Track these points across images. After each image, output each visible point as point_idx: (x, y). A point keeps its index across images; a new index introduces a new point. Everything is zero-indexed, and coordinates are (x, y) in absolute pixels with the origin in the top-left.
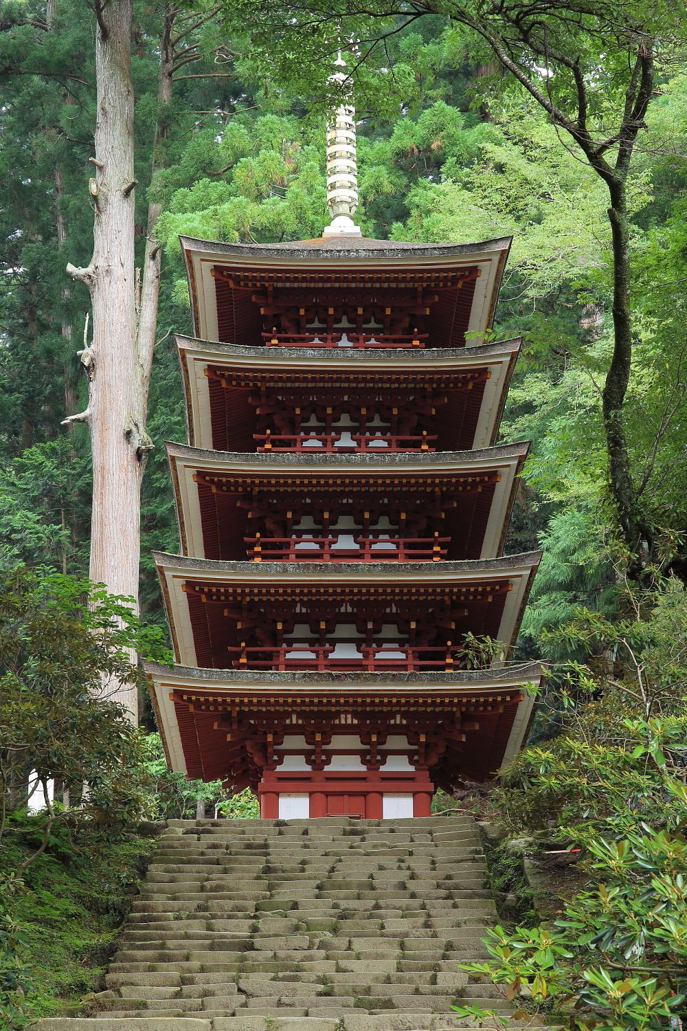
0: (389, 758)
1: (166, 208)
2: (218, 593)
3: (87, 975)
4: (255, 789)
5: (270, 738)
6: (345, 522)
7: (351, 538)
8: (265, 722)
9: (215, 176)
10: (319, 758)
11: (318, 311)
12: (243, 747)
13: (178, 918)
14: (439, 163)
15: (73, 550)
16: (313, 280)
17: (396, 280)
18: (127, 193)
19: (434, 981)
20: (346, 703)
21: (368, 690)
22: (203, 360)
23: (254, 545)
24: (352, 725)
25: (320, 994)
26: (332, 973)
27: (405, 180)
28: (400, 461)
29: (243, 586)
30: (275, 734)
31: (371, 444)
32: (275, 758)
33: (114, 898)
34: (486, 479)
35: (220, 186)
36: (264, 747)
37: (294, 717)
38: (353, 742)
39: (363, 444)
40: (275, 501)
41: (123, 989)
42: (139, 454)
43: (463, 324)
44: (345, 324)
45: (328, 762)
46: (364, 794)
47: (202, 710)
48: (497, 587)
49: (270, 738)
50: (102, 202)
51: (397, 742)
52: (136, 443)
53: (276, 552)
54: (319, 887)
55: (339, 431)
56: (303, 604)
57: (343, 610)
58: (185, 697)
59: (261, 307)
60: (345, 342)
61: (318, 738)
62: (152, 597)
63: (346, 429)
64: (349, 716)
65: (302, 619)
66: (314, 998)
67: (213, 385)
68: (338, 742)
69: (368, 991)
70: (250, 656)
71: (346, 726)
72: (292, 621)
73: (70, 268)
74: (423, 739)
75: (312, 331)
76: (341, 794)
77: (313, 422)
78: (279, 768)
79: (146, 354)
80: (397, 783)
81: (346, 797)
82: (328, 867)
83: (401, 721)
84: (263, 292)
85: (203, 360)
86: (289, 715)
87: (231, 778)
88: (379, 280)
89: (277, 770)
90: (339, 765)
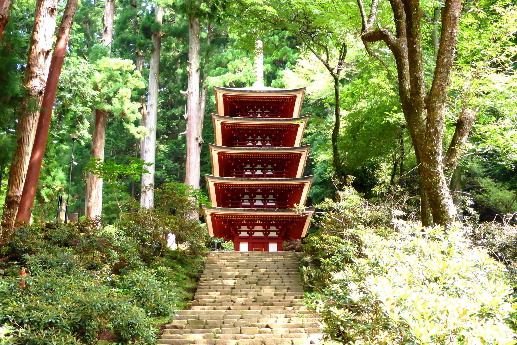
0: (257, 201)
1: (208, 75)
2: (223, 186)
3: (190, 295)
4: (233, 241)
5: (237, 227)
6: (259, 166)
7: (260, 171)
9: (223, 67)
10: (251, 232)
11: (252, 107)
13: (213, 280)
14: (285, 63)
15: (181, 171)
16: (250, 99)
17: (274, 99)
18: (197, 71)
19: (284, 298)
20: (259, 218)
23: (233, 173)
25: (253, 302)
26: (256, 296)
27: (276, 68)
29: (230, 184)
31: (266, 145)
33: (195, 274)
35: (224, 70)
38: (260, 228)
39: (264, 145)
41: (199, 300)
42: (200, 145)
44: (259, 111)
46: (264, 243)
49: (237, 227)
50: (190, 73)
51: (273, 228)
52: (199, 141)
53: (240, 174)
54: (253, 271)
55: (257, 141)
56: (247, 189)
60: (259, 116)
61: (251, 227)
62: (203, 184)
63: (259, 140)
65: (246, 193)
66: (251, 303)
67: (223, 128)
68: (257, 228)
69: (266, 301)
70: (232, 204)
72: (244, 194)
73: (181, 91)
74: (280, 227)
75: (250, 113)
77: (250, 138)
78: (240, 235)
79: (202, 116)
80: (273, 240)
82: (255, 265)
84: (236, 102)
88: (269, 99)
90: (257, 234)
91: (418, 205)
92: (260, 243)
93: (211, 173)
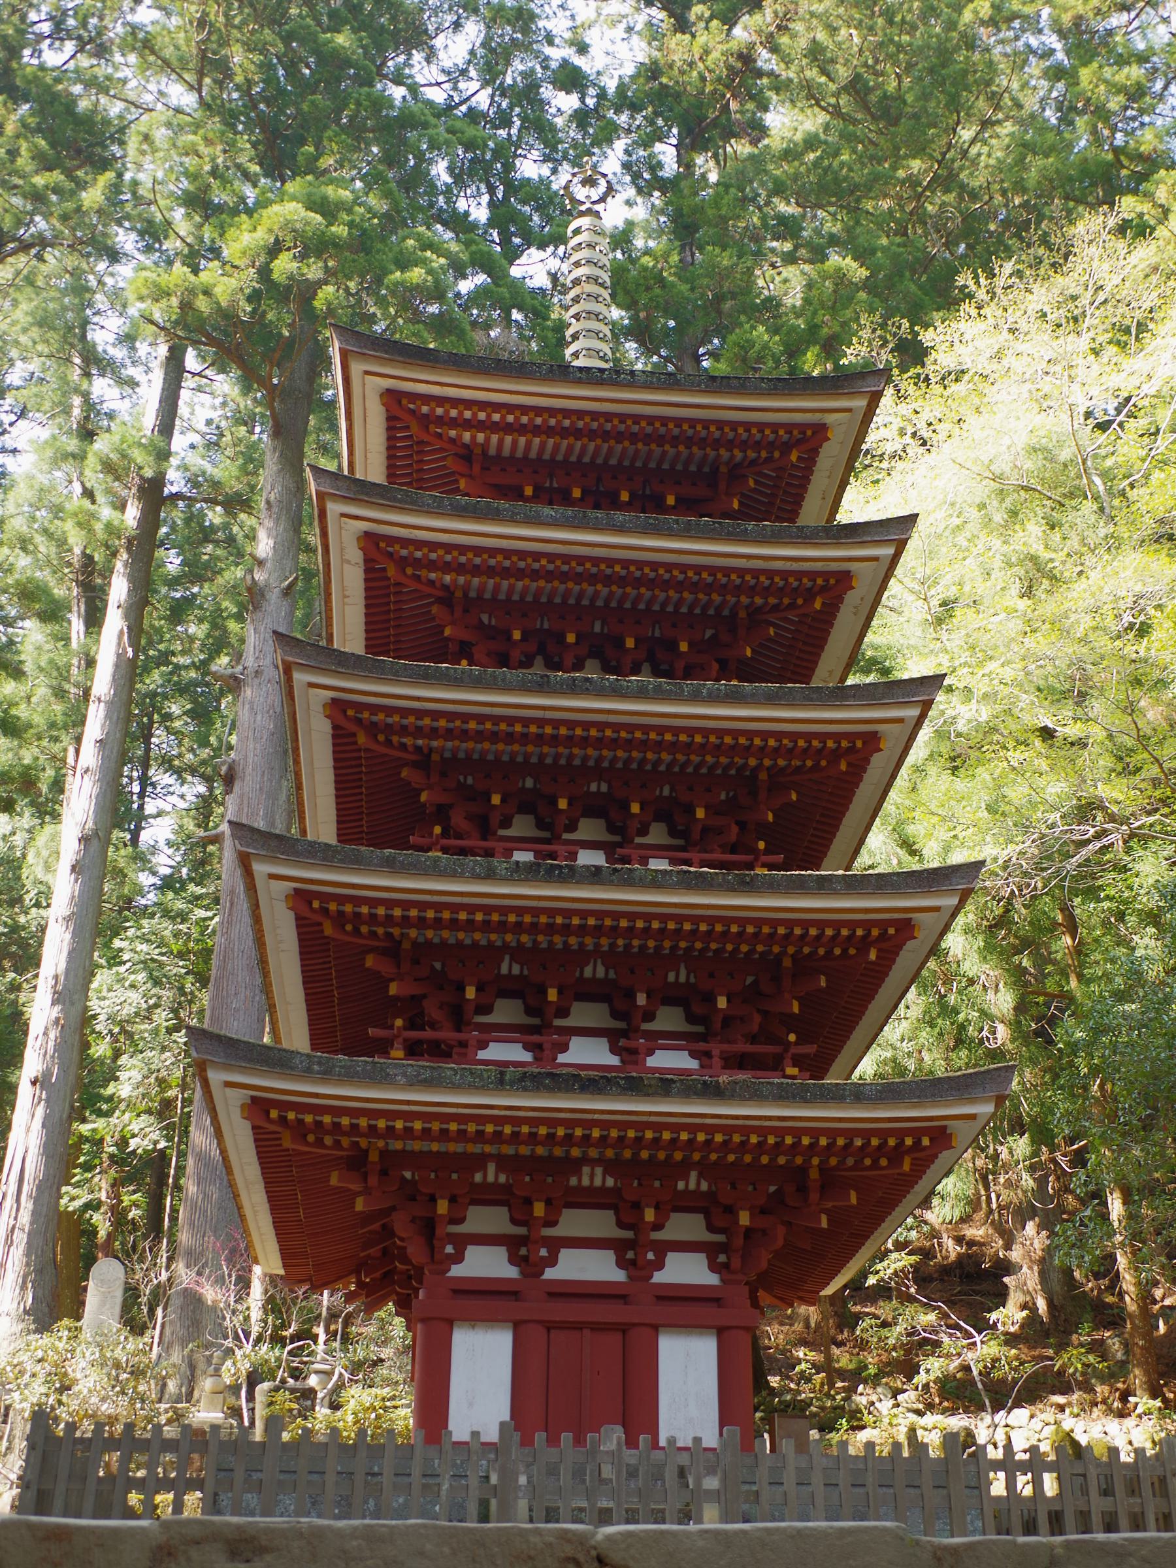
8: (433, 1175)
12: (388, 1232)
21: (650, 1113)
22: (357, 518)
24: (603, 1189)
28: (710, 695)
30: (453, 1200)
32: (449, 1249)
34: (859, 744)
36: (428, 1227)
37: (491, 1168)
38: (601, 1223)
40: (470, 780)
43: (797, 501)
45: (552, 1261)
46: (623, 1329)
47: (308, 1144)
48: (891, 931)
49: (442, 1207)
57: (588, 972)
58: (274, 1114)
59: (392, 980)
64: (599, 1171)
68: (573, 1222)
71: (591, 1190)
76: (578, 1327)
78: (456, 1271)
81: (587, 1333)
83: (698, 1184)
85: (357, 518)
86: (480, 1161)
87: (360, 1284)
89: (450, 1274)
91: (288, 299)
92: (598, 1328)
93: (368, 535)
